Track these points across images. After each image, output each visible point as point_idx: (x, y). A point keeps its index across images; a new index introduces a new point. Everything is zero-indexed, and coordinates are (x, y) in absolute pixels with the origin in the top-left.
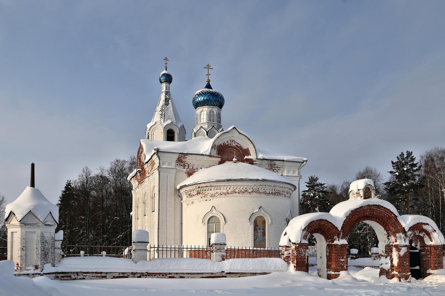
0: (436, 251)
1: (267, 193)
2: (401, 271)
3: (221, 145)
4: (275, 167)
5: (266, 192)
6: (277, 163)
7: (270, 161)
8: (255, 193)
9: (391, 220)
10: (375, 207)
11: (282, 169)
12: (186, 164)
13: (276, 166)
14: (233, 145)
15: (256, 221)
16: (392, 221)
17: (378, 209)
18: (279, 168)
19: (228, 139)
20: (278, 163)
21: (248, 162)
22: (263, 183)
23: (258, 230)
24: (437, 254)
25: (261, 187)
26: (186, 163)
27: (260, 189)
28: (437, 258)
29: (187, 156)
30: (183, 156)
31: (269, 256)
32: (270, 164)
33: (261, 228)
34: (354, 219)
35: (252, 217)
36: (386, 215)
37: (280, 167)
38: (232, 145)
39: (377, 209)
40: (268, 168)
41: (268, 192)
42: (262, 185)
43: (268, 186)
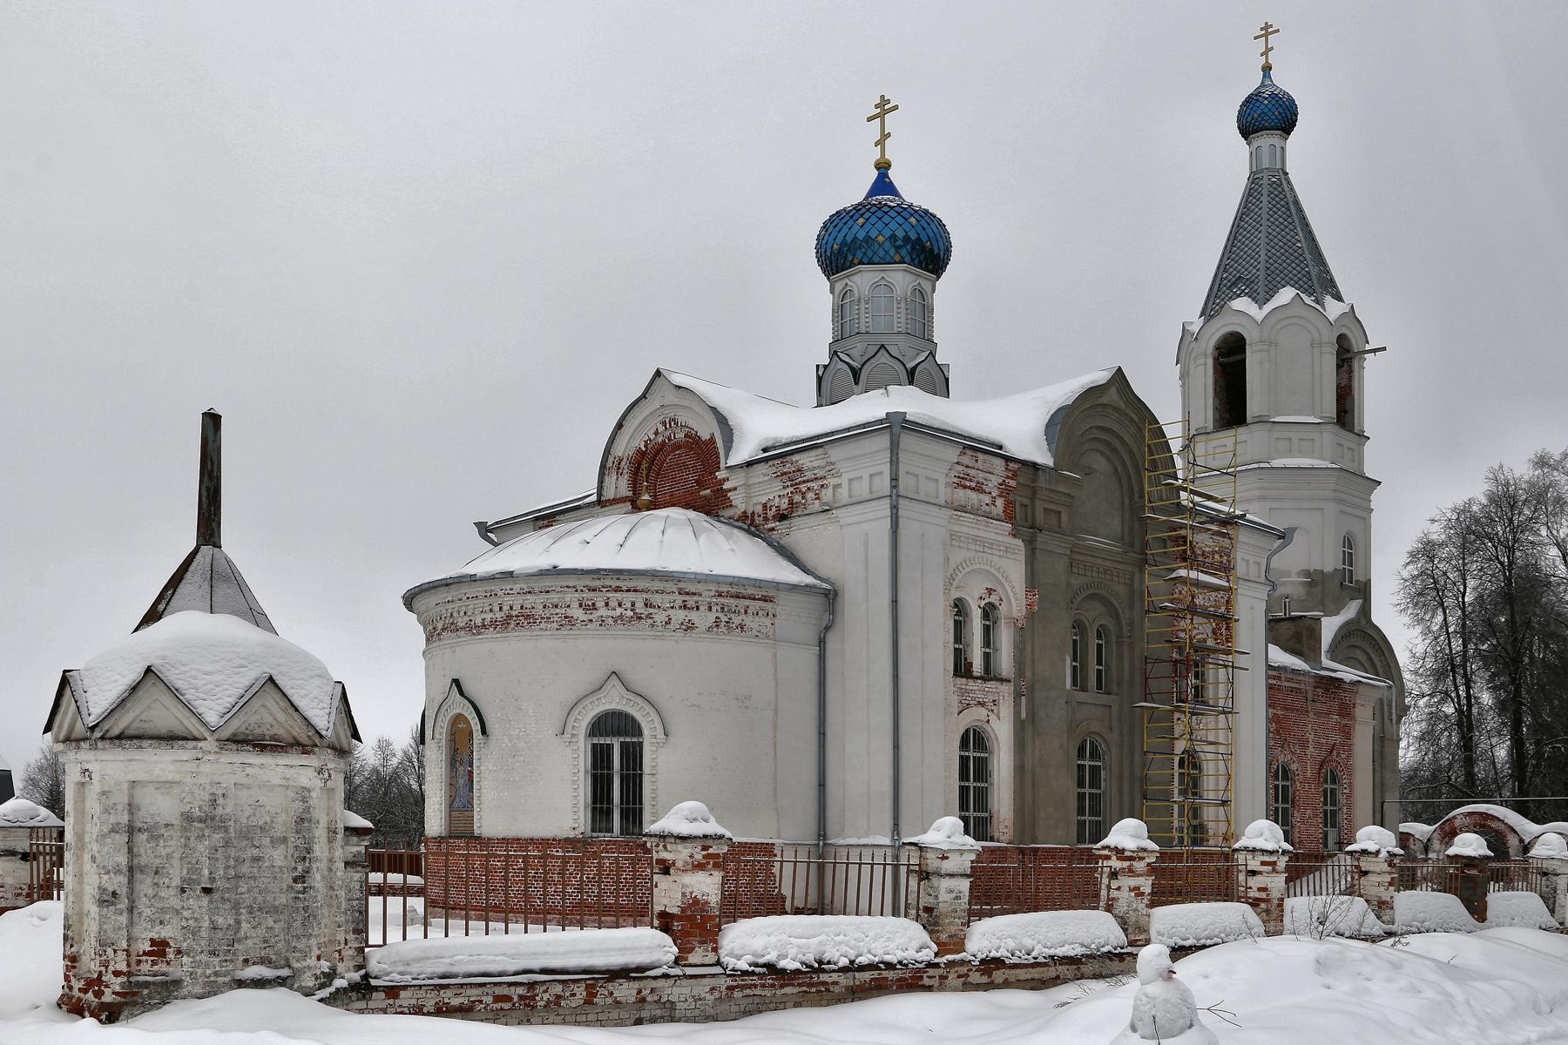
4: (808, 481)
5: (472, 623)
6: (805, 460)
7: (776, 462)
13: (809, 475)
18: (821, 478)
19: (655, 424)
37: (820, 473)
41: (479, 622)
42: (450, 599)
43: (468, 598)
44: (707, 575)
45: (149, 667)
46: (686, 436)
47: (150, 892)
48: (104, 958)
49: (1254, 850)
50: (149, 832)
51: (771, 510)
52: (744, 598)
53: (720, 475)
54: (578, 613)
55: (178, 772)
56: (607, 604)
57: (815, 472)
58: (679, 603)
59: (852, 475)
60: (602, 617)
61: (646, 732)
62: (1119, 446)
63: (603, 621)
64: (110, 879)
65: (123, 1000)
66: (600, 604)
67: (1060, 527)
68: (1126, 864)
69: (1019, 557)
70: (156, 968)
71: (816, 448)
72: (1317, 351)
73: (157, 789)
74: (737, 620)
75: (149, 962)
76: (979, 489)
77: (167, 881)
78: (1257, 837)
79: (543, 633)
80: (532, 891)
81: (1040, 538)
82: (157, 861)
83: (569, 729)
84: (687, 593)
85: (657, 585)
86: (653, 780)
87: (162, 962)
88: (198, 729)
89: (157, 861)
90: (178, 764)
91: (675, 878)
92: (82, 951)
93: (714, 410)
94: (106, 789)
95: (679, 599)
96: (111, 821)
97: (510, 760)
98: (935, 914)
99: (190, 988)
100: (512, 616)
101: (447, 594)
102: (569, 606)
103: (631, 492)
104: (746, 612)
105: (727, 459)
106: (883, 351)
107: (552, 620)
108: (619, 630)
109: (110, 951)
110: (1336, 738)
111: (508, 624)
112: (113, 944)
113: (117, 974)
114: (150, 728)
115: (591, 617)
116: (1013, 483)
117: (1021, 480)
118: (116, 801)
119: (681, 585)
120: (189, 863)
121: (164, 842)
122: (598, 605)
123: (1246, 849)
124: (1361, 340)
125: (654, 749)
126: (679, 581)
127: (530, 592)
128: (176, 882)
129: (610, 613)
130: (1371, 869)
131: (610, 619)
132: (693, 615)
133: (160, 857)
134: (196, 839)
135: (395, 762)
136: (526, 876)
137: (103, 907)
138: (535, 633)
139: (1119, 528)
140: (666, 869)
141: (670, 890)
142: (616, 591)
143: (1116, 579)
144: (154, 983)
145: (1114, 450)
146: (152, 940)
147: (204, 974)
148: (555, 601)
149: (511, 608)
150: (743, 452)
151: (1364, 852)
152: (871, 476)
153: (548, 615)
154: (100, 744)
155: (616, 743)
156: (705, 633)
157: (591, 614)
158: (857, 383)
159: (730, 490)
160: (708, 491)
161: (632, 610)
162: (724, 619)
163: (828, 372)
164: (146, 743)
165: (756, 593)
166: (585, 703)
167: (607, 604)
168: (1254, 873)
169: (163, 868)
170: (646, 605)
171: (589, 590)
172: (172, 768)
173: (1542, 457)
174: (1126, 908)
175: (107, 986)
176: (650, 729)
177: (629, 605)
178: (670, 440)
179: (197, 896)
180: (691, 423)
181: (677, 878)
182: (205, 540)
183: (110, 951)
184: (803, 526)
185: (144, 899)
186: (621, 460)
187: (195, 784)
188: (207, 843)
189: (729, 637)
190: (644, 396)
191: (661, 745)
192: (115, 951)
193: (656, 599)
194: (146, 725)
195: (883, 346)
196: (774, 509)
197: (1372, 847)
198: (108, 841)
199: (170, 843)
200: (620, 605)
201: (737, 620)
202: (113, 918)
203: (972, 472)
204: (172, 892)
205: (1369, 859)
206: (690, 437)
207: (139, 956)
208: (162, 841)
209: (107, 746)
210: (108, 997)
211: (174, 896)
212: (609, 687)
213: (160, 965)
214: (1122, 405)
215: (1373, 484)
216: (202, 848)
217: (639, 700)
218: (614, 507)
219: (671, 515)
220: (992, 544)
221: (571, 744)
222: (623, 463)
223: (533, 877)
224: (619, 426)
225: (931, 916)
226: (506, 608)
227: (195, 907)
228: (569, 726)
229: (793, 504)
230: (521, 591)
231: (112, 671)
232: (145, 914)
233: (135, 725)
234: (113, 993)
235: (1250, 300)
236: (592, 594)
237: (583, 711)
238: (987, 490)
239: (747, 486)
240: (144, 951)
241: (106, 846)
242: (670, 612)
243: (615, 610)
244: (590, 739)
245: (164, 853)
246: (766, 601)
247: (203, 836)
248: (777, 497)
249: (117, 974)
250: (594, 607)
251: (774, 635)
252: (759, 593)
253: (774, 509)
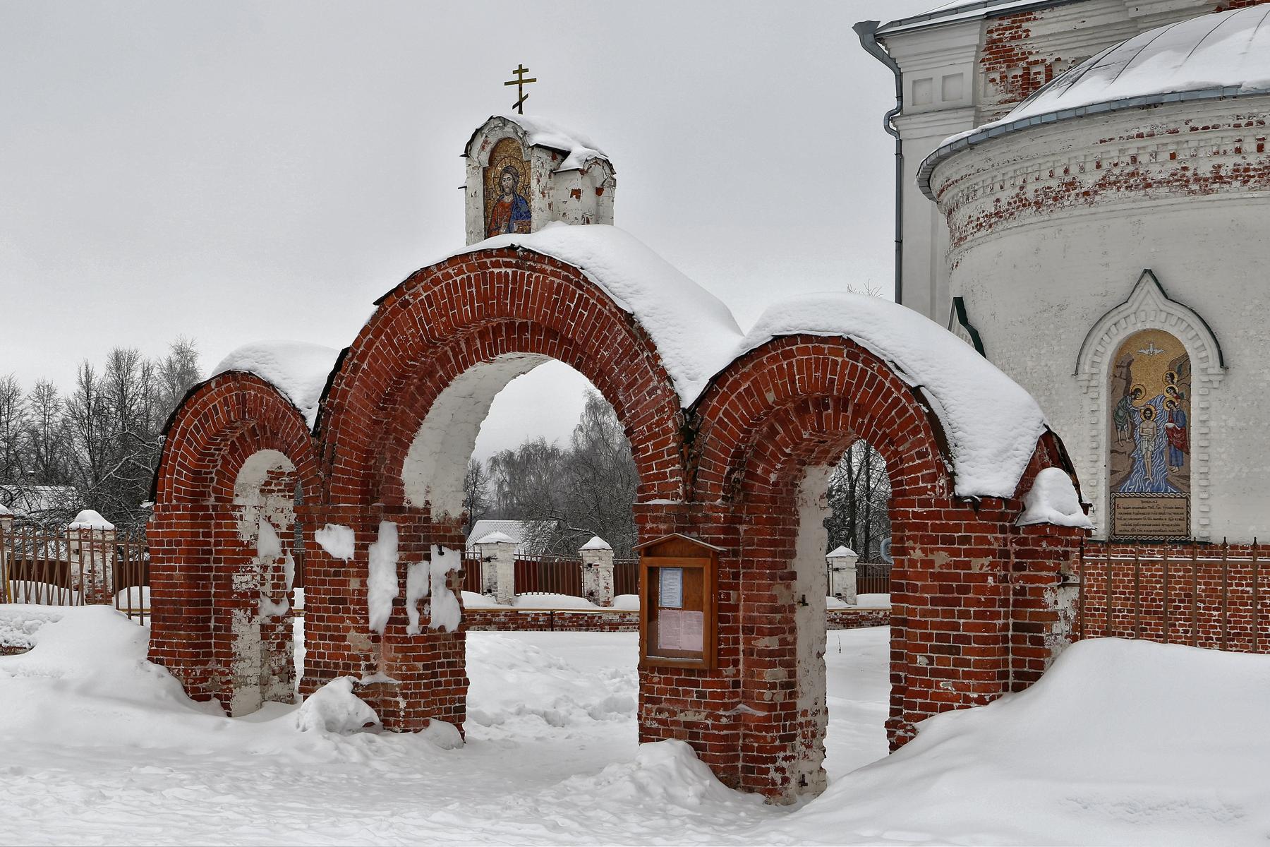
0: (924, 551)
1: (1197, 180)
2: (660, 691)
5: (1189, 174)
8: (1119, 189)
9: (606, 337)
10: (508, 265)
12: (1034, 70)
15: (1129, 364)
16: (612, 344)
17: (527, 273)
22: (1157, 122)
23: (1138, 418)
24: (935, 576)
25: (1150, 144)
26: (1036, 62)
27: (1144, 158)
28: (934, 601)
29: (1028, 20)
30: (1011, 28)
31: (1206, 584)
33: (1162, 409)
34: (397, 352)
35: (1204, 334)
36: (577, 307)
39: (522, 274)
41: (1205, 169)
42: (1145, 131)
43: (1194, 129)
59: (918, 76)
101: (1138, 124)
135: (57, 419)
152: (944, 78)
221: (1090, 390)
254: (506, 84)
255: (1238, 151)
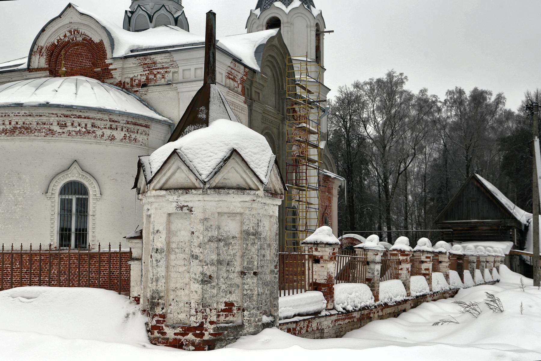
3: (53, 44)
4: (158, 69)
6: (158, 58)
7: (141, 58)
11: (173, 70)
13: (159, 66)
14: (77, 39)
18: (166, 68)
19: (65, 31)
20: (161, 59)
21: (97, 68)
32: (144, 64)
37: (166, 66)
38: (76, 40)
40: (145, 73)
44: (125, 112)
45: (175, 150)
46: (83, 39)
47: (225, 275)
48: (205, 314)
49: (423, 251)
50: (224, 241)
51: (135, 81)
52: (138, 125)
53: (107, 62)
54: (56, 128)
55: (243, 208)
56: (72, 124)
57: (163, 64)
58: (108, 126)
60: (69, 131)
61: (91, 192)
62: (276, 65)
63: (70, 133)
64: (208, 268)
65: (214, 338)
66: (69, 124)
67: (259, 100)
68: (405, 258)
69: (245, 113)
70: (227, 319)
71: (165, 53)
72: (309, 30)
73: (229, 217)
74: (133, 136)
75: (224, 315)
76: (234, 80)
77: (233, 269)
78: (423, 245)
79: (37, 138)
80: (24, 281)
81: (254, 105)
82: (229, 258)
83: (50, 191)
84: (113, 121)
85: (100, 116)
86: (94, 218)
87: (231, 315)
88: (256, 185)
89: (229, 258)
90: (242, 203)
91: (322, 265)
92: (169, 311)
93: (104, 28)
94: (207, 217)
95: (109, 124)
96: (209, 235)
97: (13, 207)
98: (372, 282)
99: (248, 329)
100: (17, 128)
102: (52, 124)
103: (48, 66)
104: (137, 133)
105: (112, 53)
106: (163, 8)
107: (41, 131)
108: (78, 138)
109: (208, 310)
110: (327, 203)
111: (14, 132)
112: (210, 306)
113: (212, 323)
114: (229, 183)
115: (64, 131)
116: (245, 78)
117: (249, 77)
118: (212, 223)
119: (111, 117)
120: (248, 258)
121: (232, 247)
122: (68, 124)
123: (419, 251)
124: (323, 27)
125: (95, 202)
126: (110, 115)
127: (30, 115)
128: (238, 269)
129: (74, 129)
130: (443, 260)
131: (74, 133)
132: (115, 133)
133: (230, 255)
134: (251, 245)
136: (21, 272)
137: (205, 285)
138: (32, 138)
139: (274, 103)
140: (317, 260)
141: (319, 271)
142: (79, 118)
143: (274, 126)
144: (229, 327)
145: (274, 66)
146: (226, 303)
147: (255, 321)
148: (44, 121)
149: (17, 123)
150: (121, 51)
151: (440, 253)
152: (195, 69)
153: (39, 128)
154: (209, 191)
155: (74, 198)
156: (119, 142)
157: (64, 129)
158: (151, 22)
159: (112, 70)
160: (99, 69)
161: (85, 128)
162: (128, 135)
163: (134, 15)
164: (231, 191)
165: (143, 123)
166: (60, 177)
167: (72, 124)
168: (423, 262)
169: (231, 261)
170: (92, 126)
171: (64, 116)
172: (239, 205)
173: (357, 83)
174: (405, 278)
175: (206, 330)
176: (92, 190)
177: (84, 125)
178: (73, 40)
179: (252, 277)
180: (88, 33)
181: (324, 265)
182: (212, 80)
183: (208, 310)
184: (155, 91)
185: (222, 279)
186: (42, 48)
187: (250, 214)
188: (256, 247)
189: (130, 145)
190: (60, 16)
191: (98, 200)
192: (211, 310)
193: (98, 123)
194: (226, 181)
195: (163, 6)
196: (137, 81)
197: (444, 250)
198: (208, 246)
199: (235, 247)
200: (79, 125)
201: (133, 136)
202: (210, 290)
203: (233, 71)
204: (235, 275)
205: (442, 256)
206: (86, 40)
207: (219, 312)
208: (231, 247)
209: (212, 193)
210: (207, 337)
211: (237, 277)
212: (73, 168)
213: (229, 317)
214: (279, 46)
215: (326, 90)
216: (254, 250)
217: (88, 176)
218: (38, 72)
219: (78, 78)
220: (237, 106)
221: (51, 199)
222: (43, 50)
223: (25, 272)
224: (43, 30)
225: (370, 283)
226: (13, 123)
227: (251, 283)
228: (50, 188)
229: (148, 79)
230: (25, 115)
231: (205, 150)
232: (222, 288)
233: (221, 181)
234: (210, 334)
235: (282, 3)
236: (65, 119)
237: (58, 181)
238: (237, 80)
239: (123, 68)
240: (221, 309)
241: (206, 249)
242: (104, 130)
243: (76, 127)
244: (61, 196)
245: (232, 253)
246: (147, 127)
247: (255, 243)
248: (139, 75)
249: (212, 323)
250: (65, 125)
251: (148, 145)
252: (144, 123)
253: (137, 81)
254: (333, 31)
255: (4, 124)
